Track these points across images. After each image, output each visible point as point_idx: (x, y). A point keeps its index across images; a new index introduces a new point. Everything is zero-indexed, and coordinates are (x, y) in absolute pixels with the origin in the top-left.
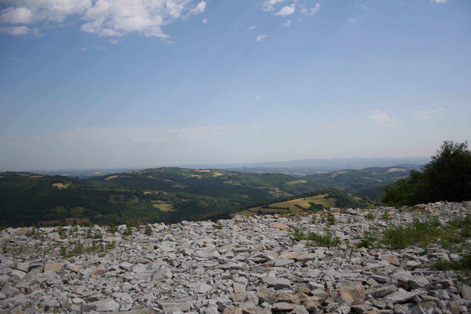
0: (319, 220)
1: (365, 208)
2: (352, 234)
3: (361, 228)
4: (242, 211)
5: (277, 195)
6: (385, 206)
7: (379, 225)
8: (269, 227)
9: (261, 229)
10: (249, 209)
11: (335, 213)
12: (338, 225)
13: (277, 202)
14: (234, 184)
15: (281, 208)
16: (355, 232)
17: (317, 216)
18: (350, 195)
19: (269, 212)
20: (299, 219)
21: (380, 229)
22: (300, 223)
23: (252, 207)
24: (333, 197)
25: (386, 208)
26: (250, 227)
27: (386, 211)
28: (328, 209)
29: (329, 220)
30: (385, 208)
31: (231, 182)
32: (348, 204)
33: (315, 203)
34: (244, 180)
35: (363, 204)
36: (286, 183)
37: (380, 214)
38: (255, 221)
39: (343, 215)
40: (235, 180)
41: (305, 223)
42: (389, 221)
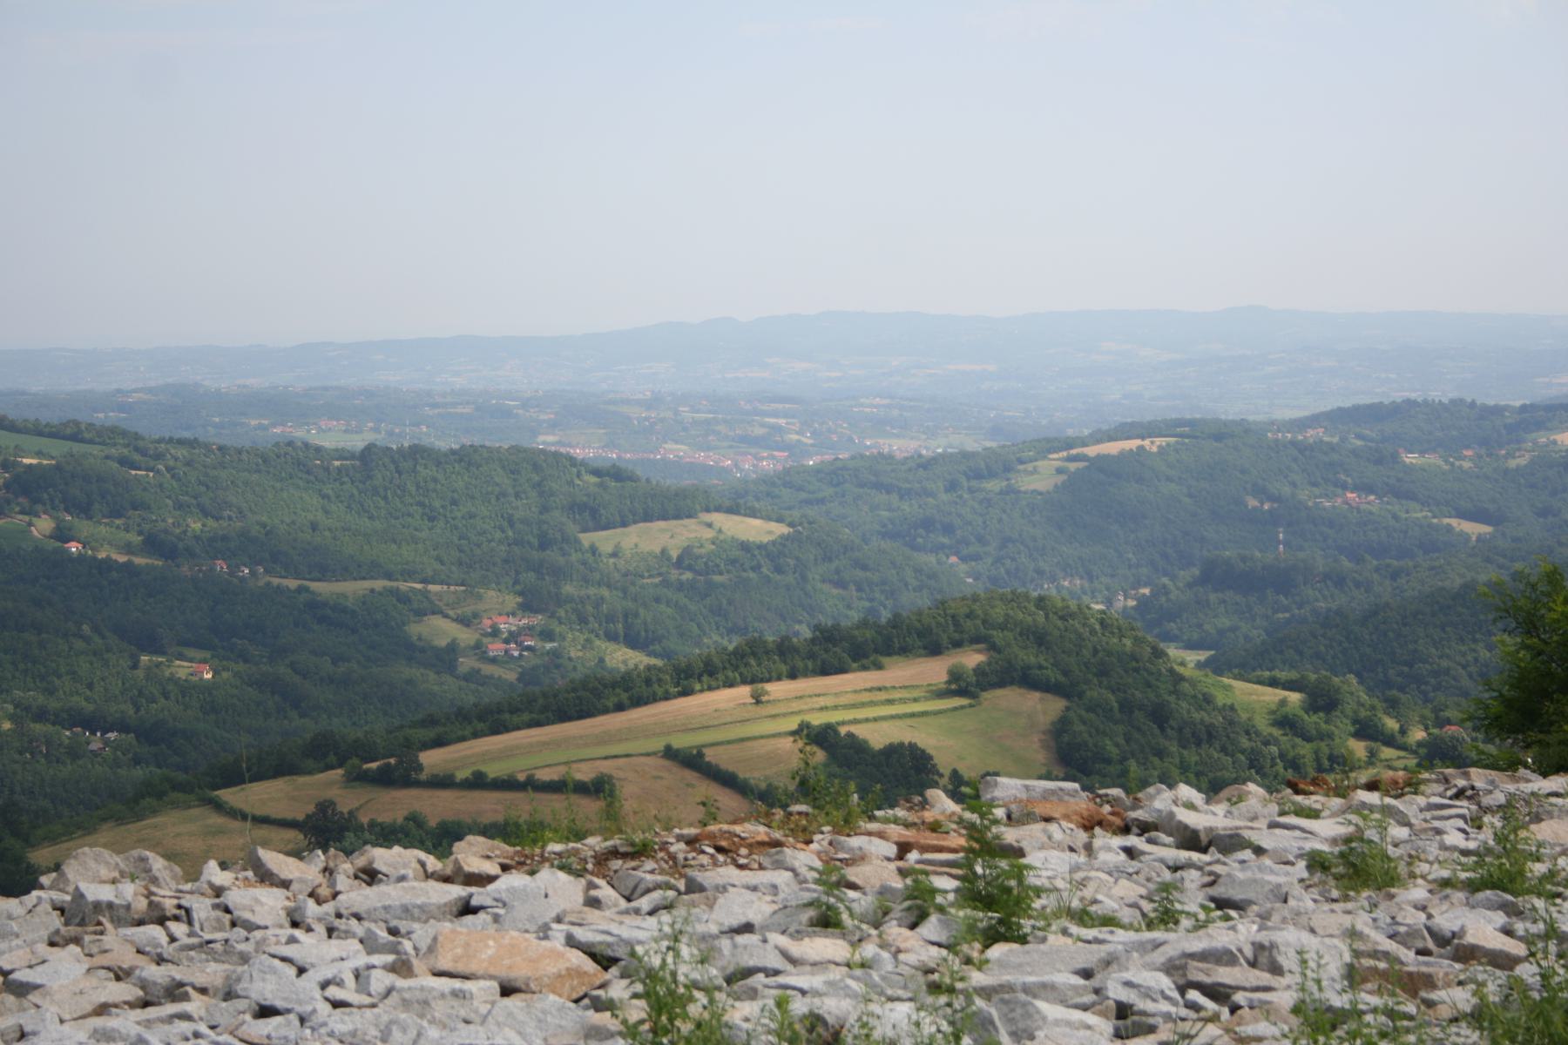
0: (884, 891)
1: (1314, 782)
2: (1185, 1027)
3: (1276, 970)
4: (155, 812)
5: (494, 660)
6: (1510, 766)
7: (1442, 940)
8: (402, 968)
9: (324, 985)
10: (228, 795)
11: (1037, 828)
12: (1055, 940)
13: (498, 729)
14: (74, 548)
15: (532, 785)
16: (1210, 1005)
17: (859, 858)
18: (1193, 657)
19: (415, 819)
20: (694, 887)
21: (1448, 985)
22: (701, 928)
23: (241, 781)
24: (1028, 680)
25: (1511, 788)
26: (212, 972)
27: (1506, 810)
28: (965, 790)
29: (974, 895)
30: (1496, 787)
31: (43, 525)
32: (1174, 748)
33: (861, 731)
34: (179, 506)
35: (1305, 750)
36: (587, 539)
37: (1454, 838)
38: (267, 904)
39: (1110, 845)
40: (84, 509)
41: (747, 928)
42: (1540, 903)
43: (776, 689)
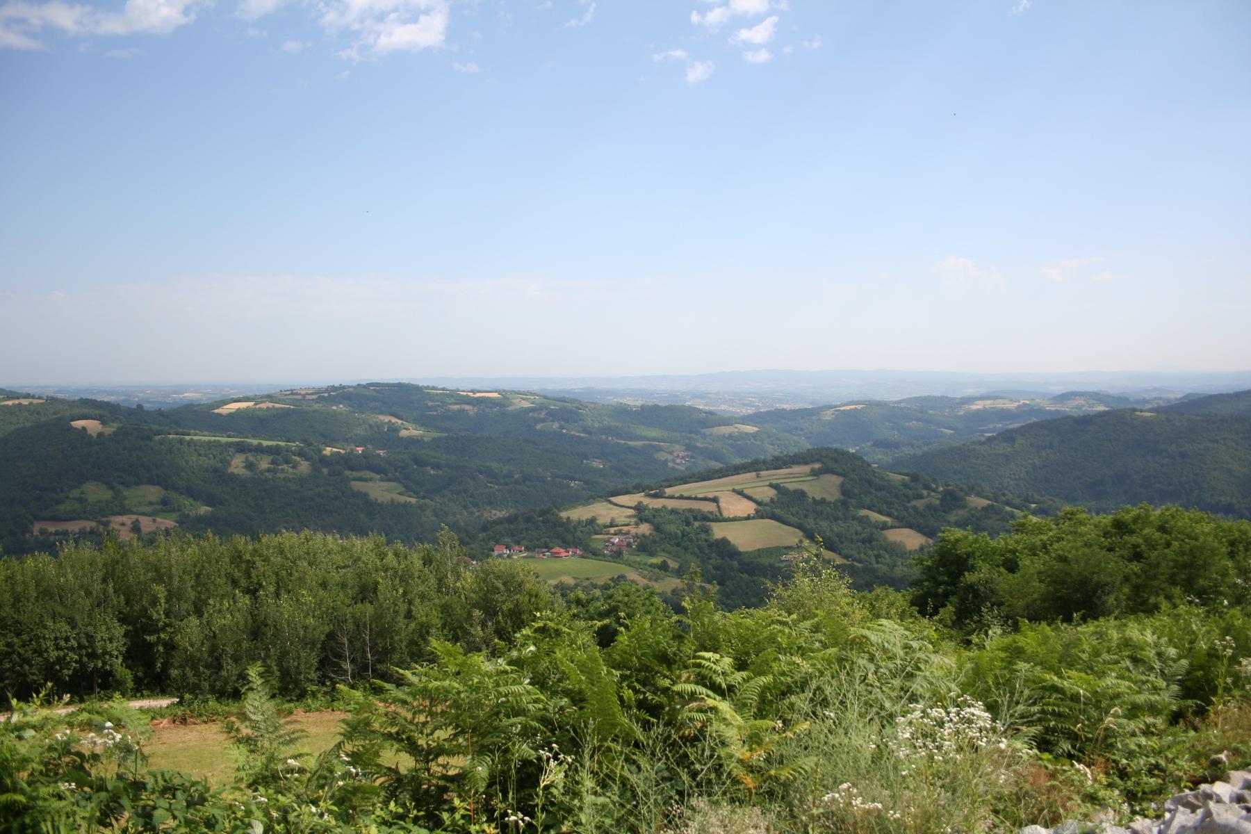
4: (593, 503)
5: (678, 464)
10: (613, 499)
14: (564, 431)
15: (696, 499)
24: (832, 472)
31: (556, 425)
33: (787, 485)
35: (910, 492)
43: (763, 473)
